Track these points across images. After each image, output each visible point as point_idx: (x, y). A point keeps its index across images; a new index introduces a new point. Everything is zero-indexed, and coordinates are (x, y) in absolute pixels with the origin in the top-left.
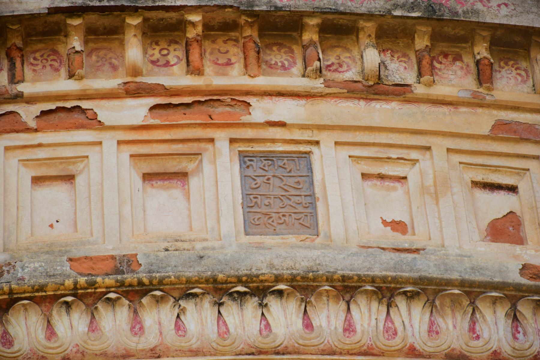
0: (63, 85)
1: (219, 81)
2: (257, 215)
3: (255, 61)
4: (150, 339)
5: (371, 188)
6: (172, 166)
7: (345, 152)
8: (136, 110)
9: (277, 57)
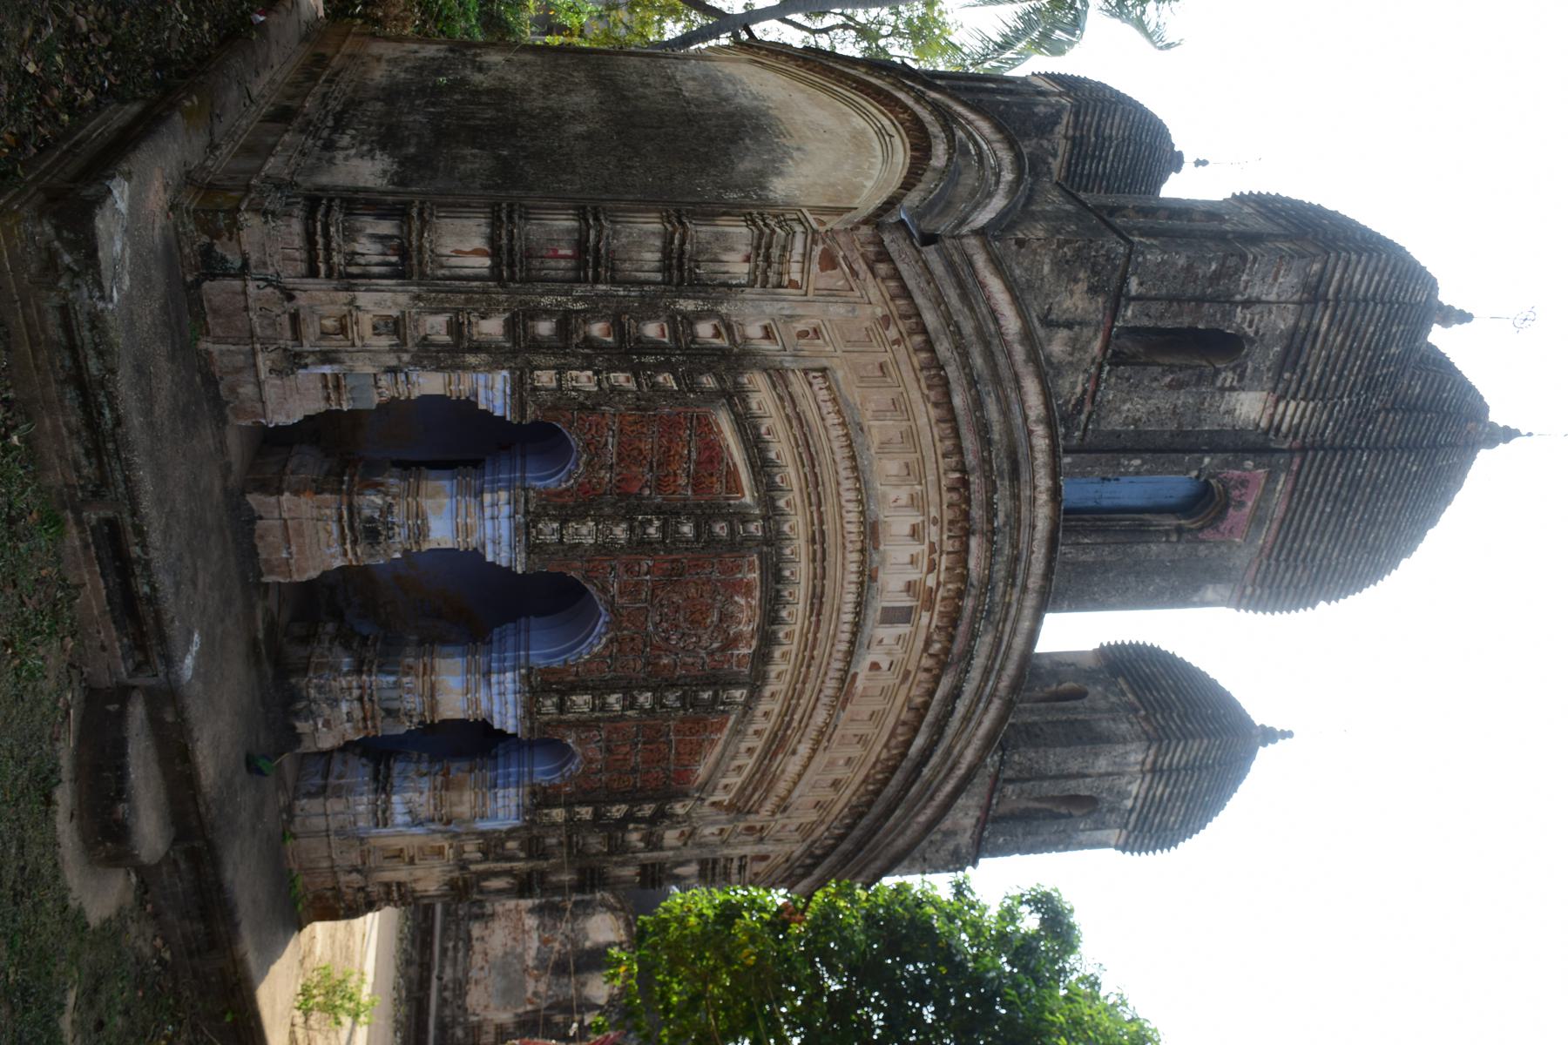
0: (943, 567)
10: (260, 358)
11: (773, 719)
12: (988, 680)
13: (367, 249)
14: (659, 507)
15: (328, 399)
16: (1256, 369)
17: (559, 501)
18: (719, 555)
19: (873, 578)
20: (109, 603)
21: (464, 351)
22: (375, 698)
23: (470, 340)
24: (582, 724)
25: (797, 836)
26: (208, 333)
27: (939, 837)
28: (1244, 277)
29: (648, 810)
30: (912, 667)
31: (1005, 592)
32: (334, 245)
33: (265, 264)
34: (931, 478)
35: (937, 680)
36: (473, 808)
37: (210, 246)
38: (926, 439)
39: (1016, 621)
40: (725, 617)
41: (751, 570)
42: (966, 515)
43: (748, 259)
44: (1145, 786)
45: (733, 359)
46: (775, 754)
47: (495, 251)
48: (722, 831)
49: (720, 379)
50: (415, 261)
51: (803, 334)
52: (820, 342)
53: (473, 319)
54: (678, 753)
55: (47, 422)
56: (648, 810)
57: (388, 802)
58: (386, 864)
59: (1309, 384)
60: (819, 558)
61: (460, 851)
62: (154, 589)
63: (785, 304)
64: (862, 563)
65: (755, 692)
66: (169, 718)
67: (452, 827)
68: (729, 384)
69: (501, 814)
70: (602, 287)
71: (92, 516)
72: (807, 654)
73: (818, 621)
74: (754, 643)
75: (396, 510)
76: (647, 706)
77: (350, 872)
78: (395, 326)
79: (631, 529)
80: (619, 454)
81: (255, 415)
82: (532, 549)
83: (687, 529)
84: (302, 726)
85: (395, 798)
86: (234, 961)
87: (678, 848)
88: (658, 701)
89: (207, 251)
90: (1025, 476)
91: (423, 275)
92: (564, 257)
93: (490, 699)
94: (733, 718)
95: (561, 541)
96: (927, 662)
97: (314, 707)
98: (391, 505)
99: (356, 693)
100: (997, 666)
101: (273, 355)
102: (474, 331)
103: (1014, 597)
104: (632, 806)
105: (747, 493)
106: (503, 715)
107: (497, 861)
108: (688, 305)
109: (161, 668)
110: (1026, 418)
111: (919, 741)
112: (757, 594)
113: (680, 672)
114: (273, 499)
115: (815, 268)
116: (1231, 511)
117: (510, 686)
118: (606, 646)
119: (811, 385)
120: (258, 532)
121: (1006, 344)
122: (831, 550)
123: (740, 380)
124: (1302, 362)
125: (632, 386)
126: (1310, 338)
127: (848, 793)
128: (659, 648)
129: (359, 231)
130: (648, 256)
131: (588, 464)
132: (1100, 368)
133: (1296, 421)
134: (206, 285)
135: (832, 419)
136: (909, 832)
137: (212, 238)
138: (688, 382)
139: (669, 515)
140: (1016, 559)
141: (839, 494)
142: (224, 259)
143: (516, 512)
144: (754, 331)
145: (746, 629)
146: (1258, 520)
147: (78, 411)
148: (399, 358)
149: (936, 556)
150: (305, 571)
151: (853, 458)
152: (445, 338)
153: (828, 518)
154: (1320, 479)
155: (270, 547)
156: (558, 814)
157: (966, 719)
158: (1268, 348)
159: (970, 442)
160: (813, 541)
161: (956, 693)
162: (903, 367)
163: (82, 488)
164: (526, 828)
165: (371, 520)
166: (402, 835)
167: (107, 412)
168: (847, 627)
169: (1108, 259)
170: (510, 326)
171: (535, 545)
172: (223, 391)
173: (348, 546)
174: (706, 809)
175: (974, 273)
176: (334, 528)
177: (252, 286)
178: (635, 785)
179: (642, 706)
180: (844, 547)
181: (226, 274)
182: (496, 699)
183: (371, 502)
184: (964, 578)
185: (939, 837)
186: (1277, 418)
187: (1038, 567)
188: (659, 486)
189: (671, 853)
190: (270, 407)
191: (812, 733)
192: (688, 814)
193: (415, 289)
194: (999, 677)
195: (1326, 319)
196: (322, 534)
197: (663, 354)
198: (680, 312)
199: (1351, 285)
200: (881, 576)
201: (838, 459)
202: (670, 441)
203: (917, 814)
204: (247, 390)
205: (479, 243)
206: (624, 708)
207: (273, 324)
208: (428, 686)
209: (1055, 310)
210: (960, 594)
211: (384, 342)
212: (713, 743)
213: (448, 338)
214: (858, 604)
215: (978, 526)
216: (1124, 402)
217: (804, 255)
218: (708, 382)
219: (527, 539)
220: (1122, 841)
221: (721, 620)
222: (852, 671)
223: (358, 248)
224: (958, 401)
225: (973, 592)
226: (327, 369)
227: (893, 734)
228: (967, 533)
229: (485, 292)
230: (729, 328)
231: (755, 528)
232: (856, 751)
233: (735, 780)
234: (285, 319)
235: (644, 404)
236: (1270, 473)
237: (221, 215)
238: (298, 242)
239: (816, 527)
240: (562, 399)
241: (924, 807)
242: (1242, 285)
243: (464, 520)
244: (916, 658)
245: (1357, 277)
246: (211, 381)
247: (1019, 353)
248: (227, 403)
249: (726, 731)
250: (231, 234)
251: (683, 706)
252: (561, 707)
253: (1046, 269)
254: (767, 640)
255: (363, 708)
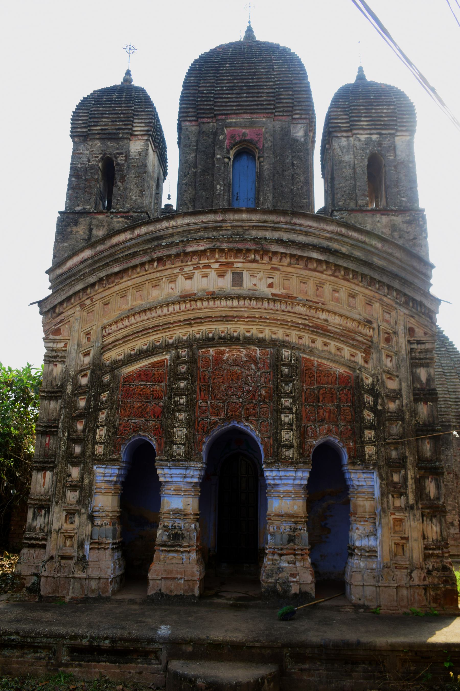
0: (206, 261)
1: (230, 260)
2: (234, 284)
3: (236, 257)
4: (216, 306)
5: (252, 278)
6: (222, 274)
7: (248, 272)
8: (217, 266)
9: (239, 255)
10: (76, 575)
11: (302, 334)
12: (279, 228)
13: (39, 522)
14: (169, 398)
15: (105, 549)
16: (118, 149)
17: (163, 445)
18: (198, 369)
19: (213, 293)
20: (115, 663)
21: (82, 485)
22: (280, 547)
23: (79, 482)
24: (302, 435)
25: (393, 313)
26: (64, 597)
27: (396, 234)
28: (79, 166)
29: (369, 399)
30: (269, 267)
31: (226, 230)
32: (34, 536)
33: (37, 566)
34: (158, 275)
35: (275, 253)
36: (367, 499)
37: (28, 588)
38: (139, 280)
39: (243, 221)
40: (236, 363)
41: (208, 352)
42: (177, 256)
43: (56, 365)
44: (361, 132)
45: (97, 368)
46: (328, 331)
47: (43, 469)
48: (388, 356)
49: (105, 373)
50: (44, 503)
51: (89, 339)
52: (92, 332)
53: (70, 480)
54: (327, 383)
55: (14, 666)
56: (369, 399)
57: (358, 547)
58: (407, 554)
59: (125, 125)
60: (200, 321)
61: (399, 509)
62: (107, 638)
63: (72, 348)
64: (202, 300)
65: (285, 344)
66: (190, 649)
67: (377, 512)
68: (108, 369)
69: (371, 483)
70: (60, 425)
71: (65, 658)
72: (257, 320)
73: (237, 317)
74: (253, 348)
75: (166, 524)
76: (291, 401)
77: (411, 577)
78: (71, 514)
79: (179, 411)
80: (140, 417)
81: (106, 583)
82: (188, 458)
83: (182, 384)
84: (295, 589)
85: (358, 544)
86: (392, 651)
87: (400, 381)
88: (287, 395)
89: (30, 590)
90: (162, 233)
91: (49, 500)
92: (49, 440)
93: (285, 485)
94: (302, 355)
95: (184, 444)
96: (266, 259)
97: (281, 581)
98: (164, 526)
99: (276, 557)
100: (272, 225)
101: (76, 569)
102: (75, 480)
103: (229, 224)
104: (365, 408)
105: (164, 357)
106: (302, 478)
107: (407, 486)
108: (69, 388)
109: (156, 645)
110: (131, 239)
111: (315, 255)
112: (222, 348)
113: (270, 385)
114: (151, 582)
115: (59, 337)
116: (247, 138)
117: (274, 474)
118: (251, 423)
119: (109, 334)
120: (168, 592)
121: (96, 255)
122: (197, 316)
123: (107, 365)
124: (115, 131)
125: (106, 411)
126: (105, 132)
127: (357, 288)
128: (254, 396)
129: (30, 525)
130: (52, 406)
131: (144, 431)
132: (112, 213)
133: (143, 125)
134: (42, 593)
135: (126, 322)
136: (390, 251)
137: (24, 587)
138: (104, 387)
139: (174, 392)
140: (206, 229)
141: (165, 315)
142: (33, 584)
143: (167, 466)
144: (87, 360)
145: (244, 352)
146: (252, 124)
147: (15, 651)
148: (83, 514)
149: (201, 266)
150: (193, 573)
151: (145, 311)
152: (77, 493)
153: (176, 318)
154: (229, 104)
155: (178, 588)
156: (370, 450)
157: (307, 234)
158: (108, 147)
159: (137, 261)
160: (190, 324)
161: (280, 242)
162: (103, 295)
163: (50, 659)
164: (379, 468)
165: (169, 536)
166: (381, 542)
167: (13, 637)
168: (242, 303)
169: (63, 221)
170: (74, 464)
171: (185, 457)
172: (93, 596)
173: (182, 549)
174: (370, 366)
175: (65, 273)
176: (171, 555)
177: (44, 574)
178: (350, 407)
179: (291, 404)
180: (193, 309)
181: (39, 584)
182: (285, 482)
183: (161, 535)
184: (213, 250)
185: (396, 234)
186: (142, 133)
187: (211, 217)
188: (159, 398)
189: (404, 385)
190: (103, 575)
191: (312, 312)
192: (372, 376)
193: (54, 503)
194: (279, 223)
195: (95, 128)
196: (174, 561)
197: (90, 398)
198: (73, 391)
199: (83, 123)
200: (211, 290)
201: (146, 318)
202: (135, 394)
203: (377, 248)
204: (94, 584)
205: (40, 476)
206: (292, 413)
207: (64, 567)
208: (277, 518)
209: (83, 237)
210: (222, 250)
211: (77, 519)
212: (320, 365)
213: (78, 491)
214: (226, 298)
215: (181, 250)
216: (131, 199)
217: (54, 342)
218: (107, 378)
219: (181, 461)
220: (407, 134)
221: (238, 365)
222: (271, 297)
223: (38, 526)
224: (116, 269)
225: (218, 244)
226: (87, 547)
227: (315, 270)
228: (186, 254)
229: (57, 474)
230: (82, 371)
231: (184, 353)
232: (327, 289)
233: (347, 352)
234: (63, 562)
235: (112, 405)
236: (226, 127)
237: (15, 581)
238: (32, 551)
239: (182, 324)
240: (113, 442)
241: (371, 245)
242: (82, 166)
243: (179, 493)
244: (264, 264)
245: (80, 122)
246: (86, 600)
247: (100, 248)
248: (99, 595)
249: (312, 358)
250: (23, 578)
251: (291, 382)
252: (290, 446)
253: (66, 244)
254: (248, 341)
255: (287, 554)
